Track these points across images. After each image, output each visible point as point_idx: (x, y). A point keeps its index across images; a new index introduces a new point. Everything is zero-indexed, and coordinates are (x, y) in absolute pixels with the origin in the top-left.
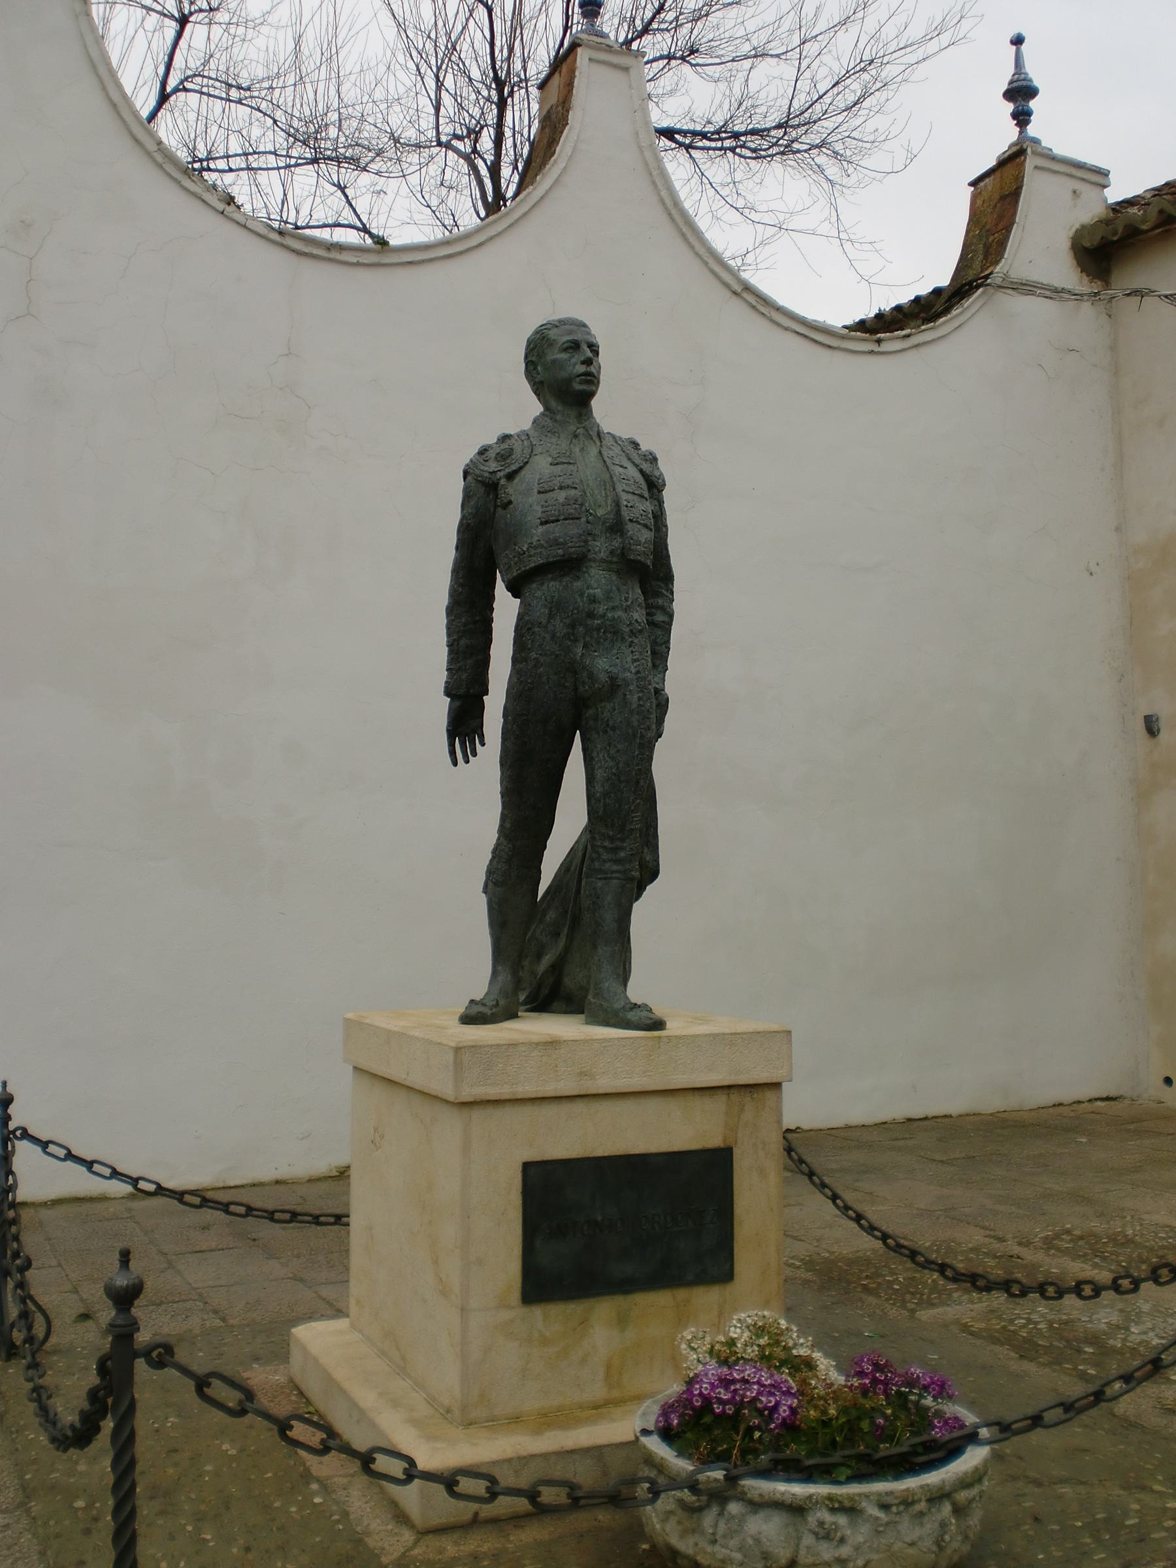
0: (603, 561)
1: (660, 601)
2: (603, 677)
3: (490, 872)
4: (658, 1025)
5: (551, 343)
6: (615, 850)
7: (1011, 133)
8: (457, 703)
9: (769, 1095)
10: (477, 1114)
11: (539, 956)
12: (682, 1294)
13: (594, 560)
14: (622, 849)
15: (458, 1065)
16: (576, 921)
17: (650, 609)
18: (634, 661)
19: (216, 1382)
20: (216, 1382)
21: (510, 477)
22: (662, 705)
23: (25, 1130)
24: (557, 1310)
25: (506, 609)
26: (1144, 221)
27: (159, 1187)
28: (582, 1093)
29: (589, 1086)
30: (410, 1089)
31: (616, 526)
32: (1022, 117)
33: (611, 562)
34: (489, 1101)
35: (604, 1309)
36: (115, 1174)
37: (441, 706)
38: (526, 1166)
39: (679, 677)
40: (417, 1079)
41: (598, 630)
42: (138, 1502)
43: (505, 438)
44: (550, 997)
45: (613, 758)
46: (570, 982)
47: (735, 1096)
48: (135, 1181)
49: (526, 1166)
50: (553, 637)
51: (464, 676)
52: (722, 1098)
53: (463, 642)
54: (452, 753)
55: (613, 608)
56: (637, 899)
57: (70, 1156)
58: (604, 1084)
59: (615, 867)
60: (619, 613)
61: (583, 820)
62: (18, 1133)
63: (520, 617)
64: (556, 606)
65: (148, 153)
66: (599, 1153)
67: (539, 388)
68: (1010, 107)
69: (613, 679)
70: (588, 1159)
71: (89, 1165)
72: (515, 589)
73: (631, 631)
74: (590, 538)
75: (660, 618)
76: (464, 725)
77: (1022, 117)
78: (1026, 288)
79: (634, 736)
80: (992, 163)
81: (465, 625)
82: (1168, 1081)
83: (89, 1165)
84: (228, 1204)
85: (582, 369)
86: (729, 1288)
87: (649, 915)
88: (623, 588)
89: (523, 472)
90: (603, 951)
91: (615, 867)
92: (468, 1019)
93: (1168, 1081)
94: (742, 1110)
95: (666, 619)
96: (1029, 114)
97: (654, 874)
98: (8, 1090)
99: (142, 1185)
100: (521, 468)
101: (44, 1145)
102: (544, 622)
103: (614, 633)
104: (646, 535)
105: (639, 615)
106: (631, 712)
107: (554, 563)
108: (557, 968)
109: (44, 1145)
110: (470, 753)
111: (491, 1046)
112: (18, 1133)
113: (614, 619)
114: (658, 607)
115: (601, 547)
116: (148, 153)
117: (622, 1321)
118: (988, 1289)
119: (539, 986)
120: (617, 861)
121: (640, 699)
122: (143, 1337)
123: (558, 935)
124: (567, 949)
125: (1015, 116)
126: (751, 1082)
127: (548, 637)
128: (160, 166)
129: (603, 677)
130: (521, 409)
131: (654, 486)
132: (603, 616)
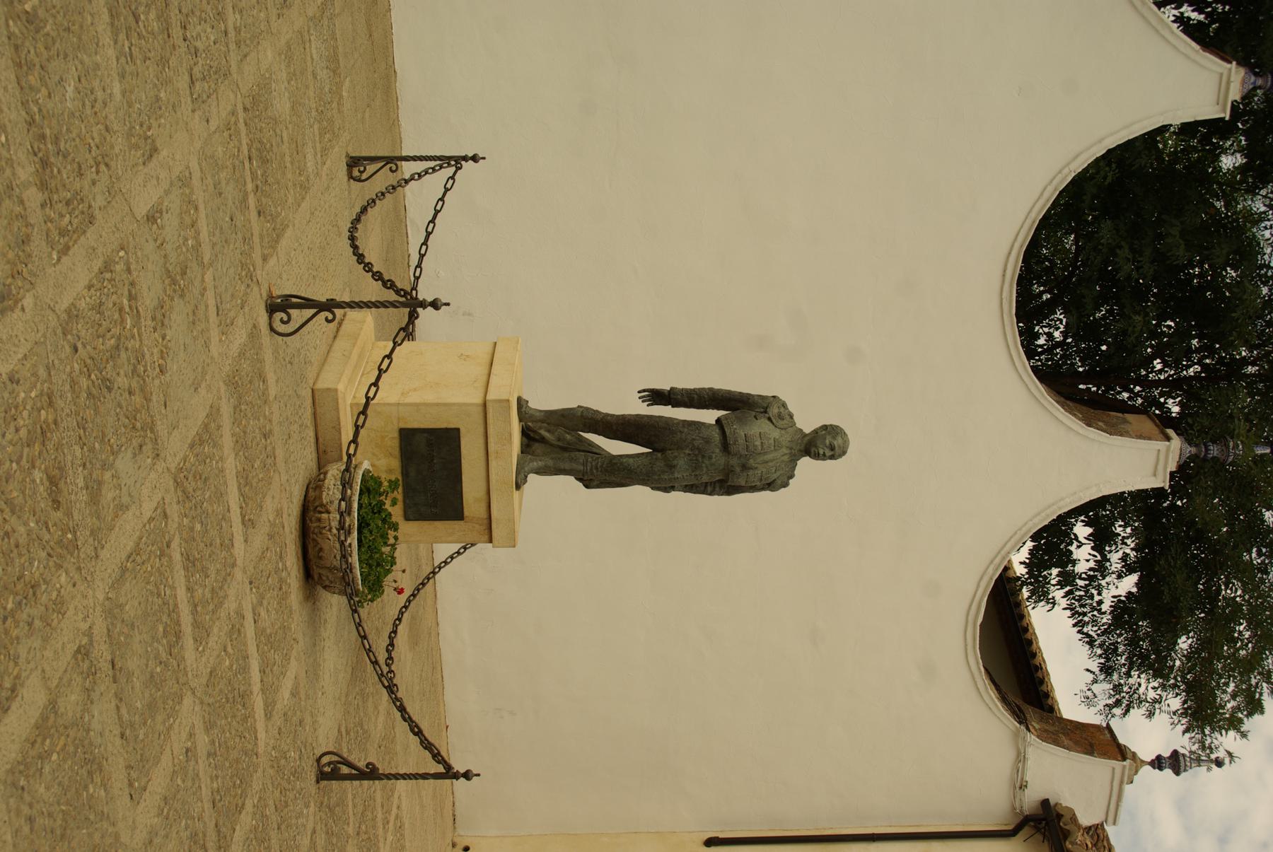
3: (587, 409)
4: (518, 487)
5: (834, 438)
7: (1147, 752)
10: (480, 409)
11: (549, 431)
15: (500, 401)
16: (564, 449)
17: (713, 484)
21: (769, 419)
22: (666, 490)
24: (396, 443)
25: (709, 416)
26: (1073, 843)
29: (490, 459)
30: (489, 375)
31: (745, 467)
32: (1158, 763)
37: (666, 387)
38: (458, 430)
39: (679, 498)
40: (494, 380)
43: (791, 416)
44: (530, 437)
46: (537, 447)
49: (458, 430)
52: (485, 515)
54: (644, 391)
58: (493, 464)
61: (614, 453)
63: (703, 424)
64: (707, 441)
65: (1068, 164)
67: (815, 432)
68: (1166, 754)
72: (718, 421)
75: (709, 489)
76: (656, 397)
77: (1158, 763)
78: (1021, 758)
80: (1122, 741)
82: (467, 849)
85: (821, 452)
87: (567, 484)
90: (550, 463)
92: (519, 399)
93: (467, 849)
96: (1161, 768)
97: (587, 487)
103: (696, 467)
104: (743, 483)
105: (705, 479)
108: (543, 440)
110: (643, 399)
115: (734, 461)
116: (1068, 164)
118: (387, 650)
119: (535, 432)
122: (420, 310)
123: (560, 441)
124: (552, 445)
125: (1159, 758)
128: (1060, 172)
130: (807, 422)
131: (771, 486)
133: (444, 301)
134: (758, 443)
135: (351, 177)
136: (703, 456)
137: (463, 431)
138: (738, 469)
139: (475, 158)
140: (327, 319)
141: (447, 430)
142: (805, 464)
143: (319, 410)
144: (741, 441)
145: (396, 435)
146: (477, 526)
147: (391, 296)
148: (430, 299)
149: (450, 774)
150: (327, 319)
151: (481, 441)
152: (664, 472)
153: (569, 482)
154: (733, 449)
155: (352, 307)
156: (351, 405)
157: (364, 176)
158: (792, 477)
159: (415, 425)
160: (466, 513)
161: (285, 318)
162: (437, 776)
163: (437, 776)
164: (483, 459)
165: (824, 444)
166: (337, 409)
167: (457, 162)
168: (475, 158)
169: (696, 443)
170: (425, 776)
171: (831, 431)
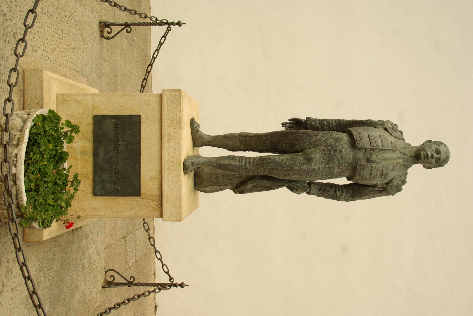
0: (356, 156)
1: (345, 194)
8: (303, 121)
9: (158, 213)
12: (91, 176)
13: (355, 153)
14: (250, 165)
15: (174, 91)
18: (319, 168)
23: (170, 30)
33: (355, 159)
34: (162, 103)
38: (139, 116)
45: (283, 160)
47: (158, 198)
49: (139, 116)
50: (327, 139)
51: (313, 123)
52: (158, 193)
53: (325, 122)
55: (338, 160)
59: (243, 163)
60: (336, 162)
62: (169, 28)
66: (142, 144)
69: (312, 159)
70: (140, 139)
71: (157, 50)
73: (330, 167)
74: (364, 151)
75: (338, 193)
79: (291, 167)
81: (332, 123)
83: (157, 50)
84: (146, 80)
86: (92, 195)
88: (346, 165)
89: (388, 133)
91: (243, 163)
92: (192, 122)
94: (153, 201)
95: (338, 196)
98: (183, 25)
100: (389, 133)
101: (165, 36)
102: (332, 136)
106: (300, 166)
107: (355, 142)
109: (165, 36)
111: (180, 102)
112: (169, 28)
113: (334, 160)
114: (342, 192)
115: (360, 155)
117: (84, 152)
120: (245, 164)
121: (305, 169)
126: (163, 204)
127: (327, 138)
129: (312, 156)
130: (414, 139)
132: (335, 155)
133: (186, 284)
134: (379, 141)
135: (102, 36)
136: (335, 151)
138: (363, 163)
139: (179, 24)
141: (131, 116)
142: (416, 171)
143: (27, 88)
144: (366, 139)
145: (90, 121)
146: (151, 202)
147: (124, 27)
148: (179, 283)
151: (157, 126)
152: (303, 164)
153: (228, 192)
154: (359, 143)
155: (143, 286)
156: (58, 95)
157: (111, 35)
158: (404, 182)
159: (106, 113)
160: (143, 190)
161: (110, 31)
164: (158, 142)
165: (431, 156)
166: (41, 88)
167: (169, 24)
168: (179, 24)
169: (329, 142)
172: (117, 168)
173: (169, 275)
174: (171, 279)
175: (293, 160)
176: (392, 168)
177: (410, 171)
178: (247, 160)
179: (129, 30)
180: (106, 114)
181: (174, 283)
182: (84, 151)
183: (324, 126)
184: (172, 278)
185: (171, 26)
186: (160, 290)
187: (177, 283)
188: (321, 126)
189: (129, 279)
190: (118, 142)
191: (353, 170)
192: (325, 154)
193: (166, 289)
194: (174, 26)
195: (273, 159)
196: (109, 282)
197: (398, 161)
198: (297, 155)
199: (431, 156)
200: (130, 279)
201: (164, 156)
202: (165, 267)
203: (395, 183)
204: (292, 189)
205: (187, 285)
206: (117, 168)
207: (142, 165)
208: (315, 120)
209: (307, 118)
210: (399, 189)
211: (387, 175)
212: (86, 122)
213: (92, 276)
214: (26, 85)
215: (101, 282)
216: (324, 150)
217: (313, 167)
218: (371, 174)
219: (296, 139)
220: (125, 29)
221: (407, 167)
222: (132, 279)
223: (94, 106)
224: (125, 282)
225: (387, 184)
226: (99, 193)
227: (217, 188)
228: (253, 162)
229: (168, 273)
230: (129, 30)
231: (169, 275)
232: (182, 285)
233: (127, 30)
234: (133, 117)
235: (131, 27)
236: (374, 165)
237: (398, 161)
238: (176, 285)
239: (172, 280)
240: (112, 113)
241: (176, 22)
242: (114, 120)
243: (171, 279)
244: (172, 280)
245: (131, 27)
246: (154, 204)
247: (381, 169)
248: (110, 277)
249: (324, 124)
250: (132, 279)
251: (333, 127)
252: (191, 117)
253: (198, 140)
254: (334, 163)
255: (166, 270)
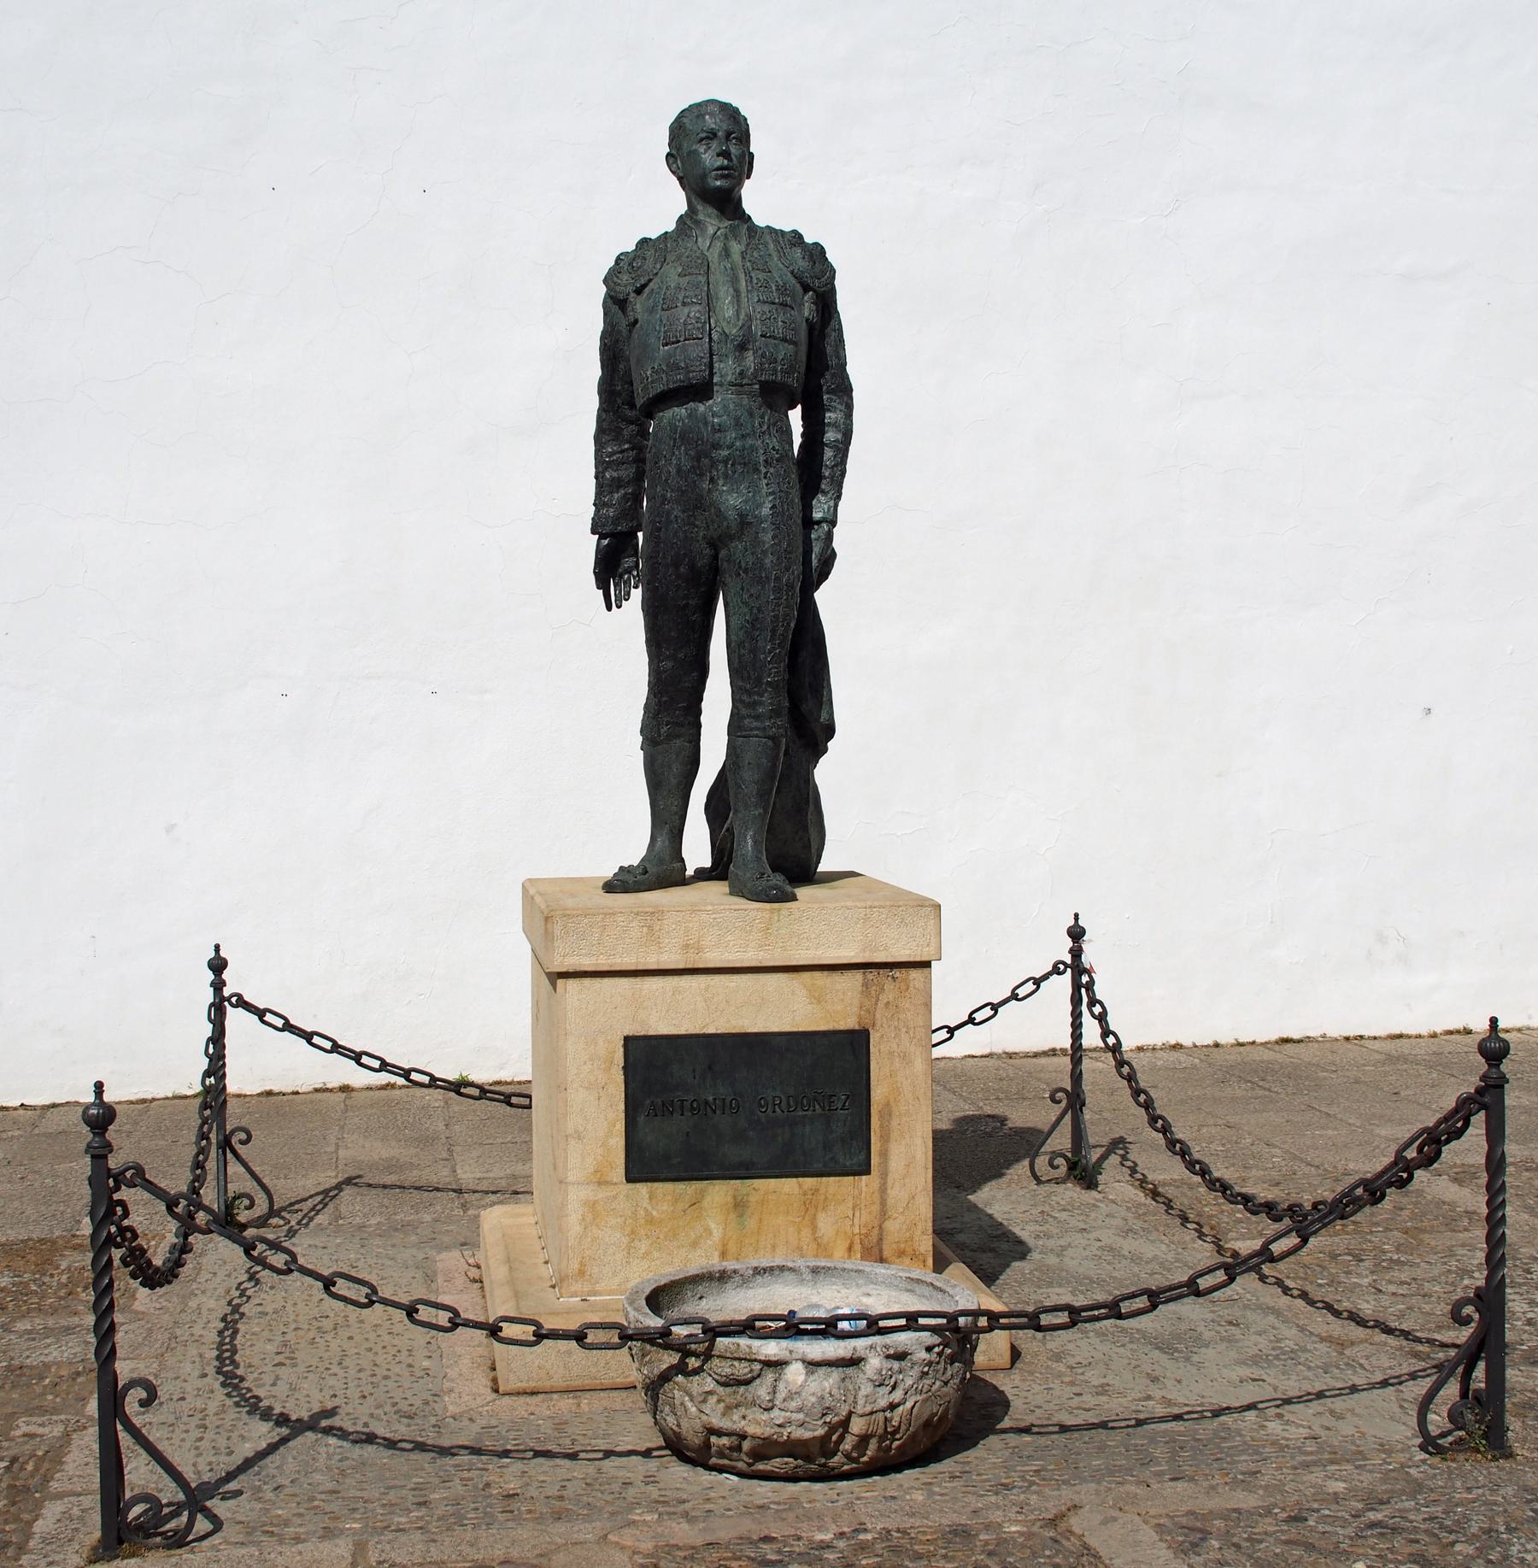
2: (732, 515)
6: (755, 704)
9: (915, 974)
12: (809, 1182)
14: (761, 703)
19: (340, 1282)
20: (340, 1282)
23: (239, 996)
27: (433, 1078)
28: (689, 966)
35: (718, 1192)
36: (385, 1066)
38: (628, 1040)
41: (725, 462)
42: (116, 1295)
45: (746, 604)
47: (872, 975)
48: (406, 1074)
49: (628, 1040)
52: (858, 976)
56: (818, 750)
57: (288, 1027)
60: (750, 442)
66: (711, 1030)
99: (414, 1076)
101: (260, 1014)
106: (764, 552)
107: (692, 386)
109: (260, 1014)
112: (234, 1000)
120: (757, 717)
130: (663, 205)
137: (627, 1033)
138: (750, 360)
139: (218, 965)
140: (145, 1404)
142: (762, 201)
145: (643, 1189)
147: (229, 1155)
148: (1069, 943)
149: (1488, 1098)
150: (145, 1404)
152: (756, 542)
158: (797, 237)
159: (618, 1142)
160: (849, 1023)
161: (246, 1202)
162: (1495, 1134)
163: (1495, 1134)
165: (711, 151)
168: (218, 965)
169: (687, 465)
170: (1496, 1164)
171: (680, 157)
172: (784, 1105)
173: (1045, 977)
174: (1056, 970)
175: (746, 571)
176: (762, 276)
177: (760, 220)
178: (744, 711)
179: (243, 1136)
180: (622, 1142)
181: (1068, 960)
182: (736, 1206)
183: (619, 479)
184: (1055, 966)
185: (226, 992)
186: (1093, 1002)
187: (1071, 951)
188: (619, 488)
189: (1057, 1110)
190: (707, 1103)
191: (775, 396)
192: (726, 476)
193: (1092, 982)
194: (224, 983)
195: (741, 633)
196: (1072, 1166)
197: (736, 257)
198: (729, 561)
199: (711, 151)
200: (1059, 1102)
201: (738, 969)
202: (979, 1017)
203: (802, 264)
204: (824, 574)
205: (1076, 916)
206: (784, 1105)
207: (774, 1027)
208: (599, 504)
209: (593, 532)
210: (817, 253)
211: (783, 290)
212: (645, 1203)
213: (1064, 1215)
214: (547, 1384)
215: (1071, 1192)
216: (712, 480)
217: (766, 511)
218: (784, 340)
219: (676, 564)
220: (238, 1147)
221: (753, 229)
222: (1060, 1095)
223: (599, 1183)
224: (1068, 1117)
225: (806, 289)
226: (862, 1157)
227: (812, 807)
228: (749, 693)
229: (1037, 982)
230: (243, 1136)
231: (1045, 977)
232: (1076, 933)
233: (242, 1142)
234: (631, 1059)
235: (229, 1128)
236: (757, 328)
237: (736, 257)
238: (1076, 953)
239: (1062, 967)
240: (620, 1126)
241: (211, 976)
242: (641, 1119)
243: (1056, 970)
244: (1062, 967)
245: (229, 1128)
246: (889, 987)
247: (766, 308)
248: (1057, 1167)
249: (613, 479)
250: (1060, 1095)
251: (622, 452)
252: (601, 892)
253: (661, 870)
254: (753, 449)
255: (1030, 987)
